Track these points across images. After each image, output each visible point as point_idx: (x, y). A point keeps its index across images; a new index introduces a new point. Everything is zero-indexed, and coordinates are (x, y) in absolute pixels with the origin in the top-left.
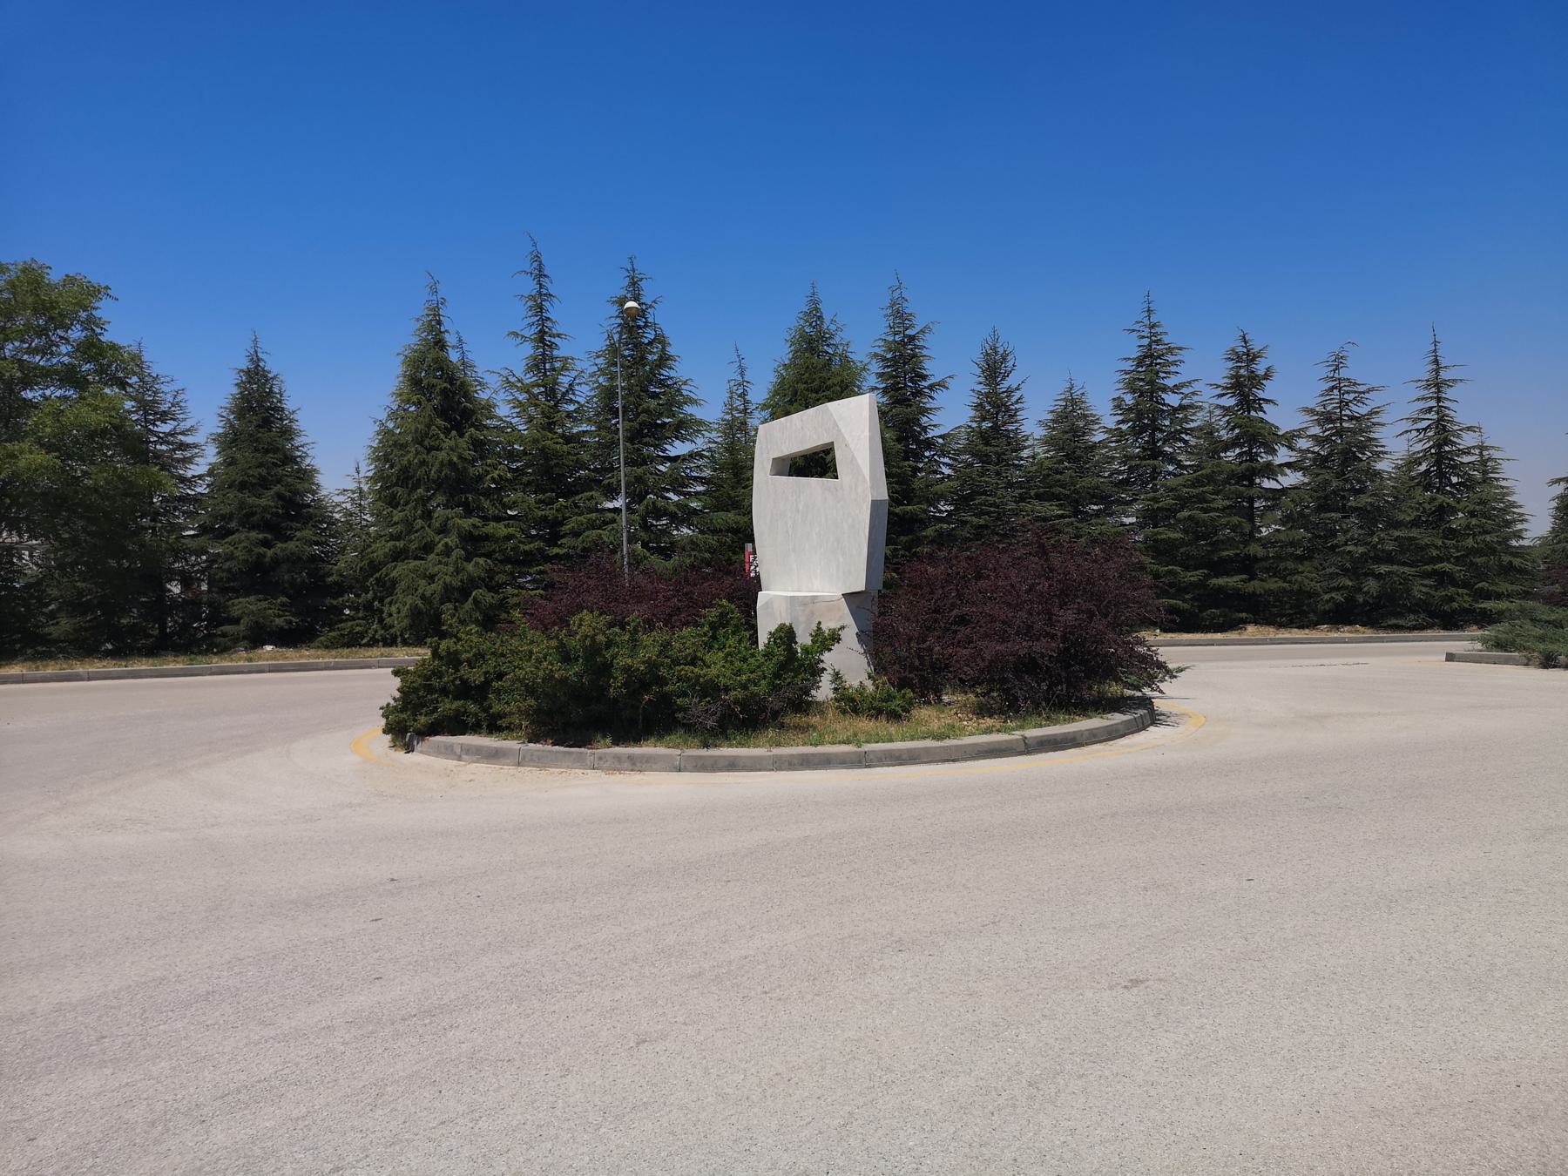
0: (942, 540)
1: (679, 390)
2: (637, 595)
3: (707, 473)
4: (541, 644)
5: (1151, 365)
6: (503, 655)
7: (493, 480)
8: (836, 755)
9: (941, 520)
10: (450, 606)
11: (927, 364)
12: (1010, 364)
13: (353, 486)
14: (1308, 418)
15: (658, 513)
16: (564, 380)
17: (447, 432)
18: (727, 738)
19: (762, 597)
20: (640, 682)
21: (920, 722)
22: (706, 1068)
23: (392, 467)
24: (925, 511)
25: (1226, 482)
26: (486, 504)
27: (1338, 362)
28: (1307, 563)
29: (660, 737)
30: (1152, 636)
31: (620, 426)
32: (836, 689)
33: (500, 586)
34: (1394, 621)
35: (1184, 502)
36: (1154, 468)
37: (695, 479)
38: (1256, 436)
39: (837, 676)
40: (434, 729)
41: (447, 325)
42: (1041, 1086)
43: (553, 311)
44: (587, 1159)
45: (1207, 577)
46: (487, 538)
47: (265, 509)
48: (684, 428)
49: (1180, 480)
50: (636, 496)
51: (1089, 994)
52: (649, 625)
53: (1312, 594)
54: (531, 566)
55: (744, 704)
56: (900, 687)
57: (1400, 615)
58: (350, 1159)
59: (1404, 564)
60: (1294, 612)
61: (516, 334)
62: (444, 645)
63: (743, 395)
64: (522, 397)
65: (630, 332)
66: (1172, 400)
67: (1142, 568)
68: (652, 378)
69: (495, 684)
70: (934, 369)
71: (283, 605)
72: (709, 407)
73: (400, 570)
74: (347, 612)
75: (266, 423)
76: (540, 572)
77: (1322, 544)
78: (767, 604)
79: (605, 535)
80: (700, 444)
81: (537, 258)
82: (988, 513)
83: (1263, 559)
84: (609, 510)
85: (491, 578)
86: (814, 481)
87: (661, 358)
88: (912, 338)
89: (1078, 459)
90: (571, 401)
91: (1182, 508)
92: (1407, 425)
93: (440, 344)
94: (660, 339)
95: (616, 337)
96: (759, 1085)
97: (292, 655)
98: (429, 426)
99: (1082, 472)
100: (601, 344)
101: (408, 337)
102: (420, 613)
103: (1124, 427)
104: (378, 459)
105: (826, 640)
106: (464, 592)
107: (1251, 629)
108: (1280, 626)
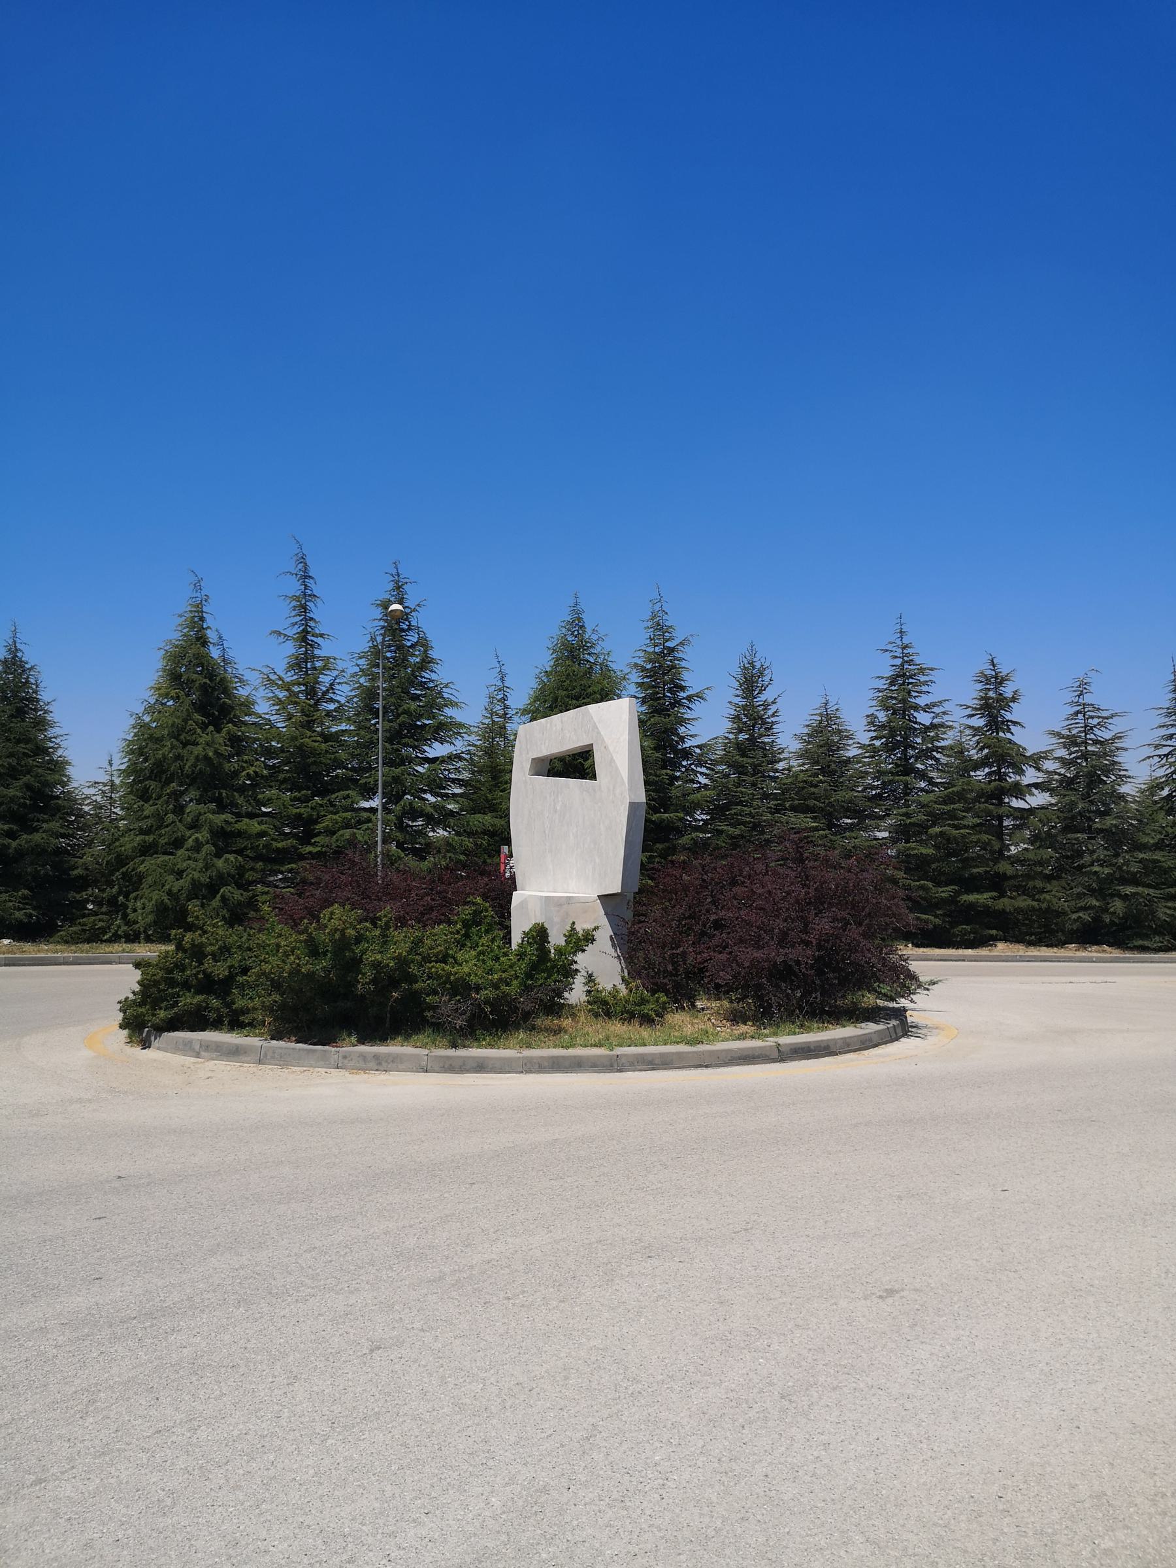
0: (698, 848)
1: (440, 693)
2: (389, 893)
3: (465, 775)
4: (291, 939)
5: (904, 683)
6: (250, 949)
7: (249, 776)
8: (588, 1058)
9: (697, 829)
10: (197, 902)
11: (685, 675)
12: (767, 678)
13: (105, 778)
14: (1054, 740)
15: (414, 814)
16: (325, 679)
17: (204, 727)
18: (477, 1040)
19: (517, 897)
20: (388, 980)
21: (672, 1027)
22: (443, 1377)
23: (146, 760)
24: (682, 820)
25: (976, 800)
26: (240, 800)
27: (1082, 688)
28: (1054, 882)
29: (407, 1037)
30: (908, 950)
31: (379, 726)
32: (589, 992)
33: (251, 883)
34: (1140, 942)
35: (936, 819)
36: (906, 784)
37: (453, 781)
38: (1005, 757)
39: (590, 978)
40: (173, 1025)
41: (209, 622)
42: (794, 1398)
43: (316, 612)
44: (312, 1472)
45: (957, 893)
46: (240, 834)
47: (12, 799)
48: (443, 730)
49: (931, 796)
50: (393, 797)
51: (843, 1303)
52: (402, 922)
53: (1060, 914)
54: (282, 864)
55: (494, 1004)
56: (653, 992)
57: (1146, 937)
58: (54, 1470)
59: (1149, 886)
60: (1042, 930)
61: (280, 634)
62: (189, 937)
63: (503, 700)
64: (282, 695)
65: (394, 635)
66: (924, 718)
67: (894, 881)
68: (412, 681)
69: (240, 979)
70: (692, 680)
71: (24, 897)
72: (470, 710)
73: (147, 865)
74: (90, 907)
75: (20, 713)
76: (290, 871)
77: (1070, 864)
78: (524, 904)
79: (360, 835)
80: (458, 746)
81: (302, 559)
82: (744, 823)
83: (1011, 877)
84: (365, 809)
85: (241, 876)
86: (573, 783)
87: (423, 661)
88: (672, 650)
89: (833, 773)
90: (332, 700)
91: (934, 825)
92: (1150, 751)
93: (203, 641)
94: (423, 643)
95: (379, 639)
96: (498, 1396)
97: (30, 949)
98: (185, 721)
99: (836, 786)
100: (364, 645)
101: (171, 632)
102: (166, 909)
103: (877, 743)
104: (132, 752)
105: (580, 941)
106: (212, 889)
107: (1001, 945)
108: (1030, 944)
